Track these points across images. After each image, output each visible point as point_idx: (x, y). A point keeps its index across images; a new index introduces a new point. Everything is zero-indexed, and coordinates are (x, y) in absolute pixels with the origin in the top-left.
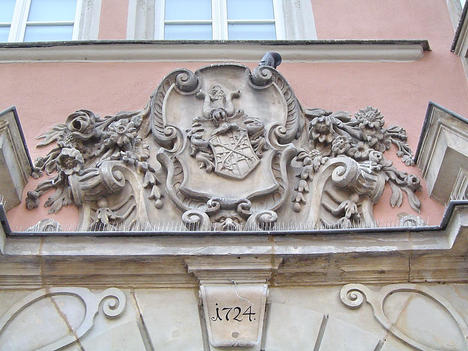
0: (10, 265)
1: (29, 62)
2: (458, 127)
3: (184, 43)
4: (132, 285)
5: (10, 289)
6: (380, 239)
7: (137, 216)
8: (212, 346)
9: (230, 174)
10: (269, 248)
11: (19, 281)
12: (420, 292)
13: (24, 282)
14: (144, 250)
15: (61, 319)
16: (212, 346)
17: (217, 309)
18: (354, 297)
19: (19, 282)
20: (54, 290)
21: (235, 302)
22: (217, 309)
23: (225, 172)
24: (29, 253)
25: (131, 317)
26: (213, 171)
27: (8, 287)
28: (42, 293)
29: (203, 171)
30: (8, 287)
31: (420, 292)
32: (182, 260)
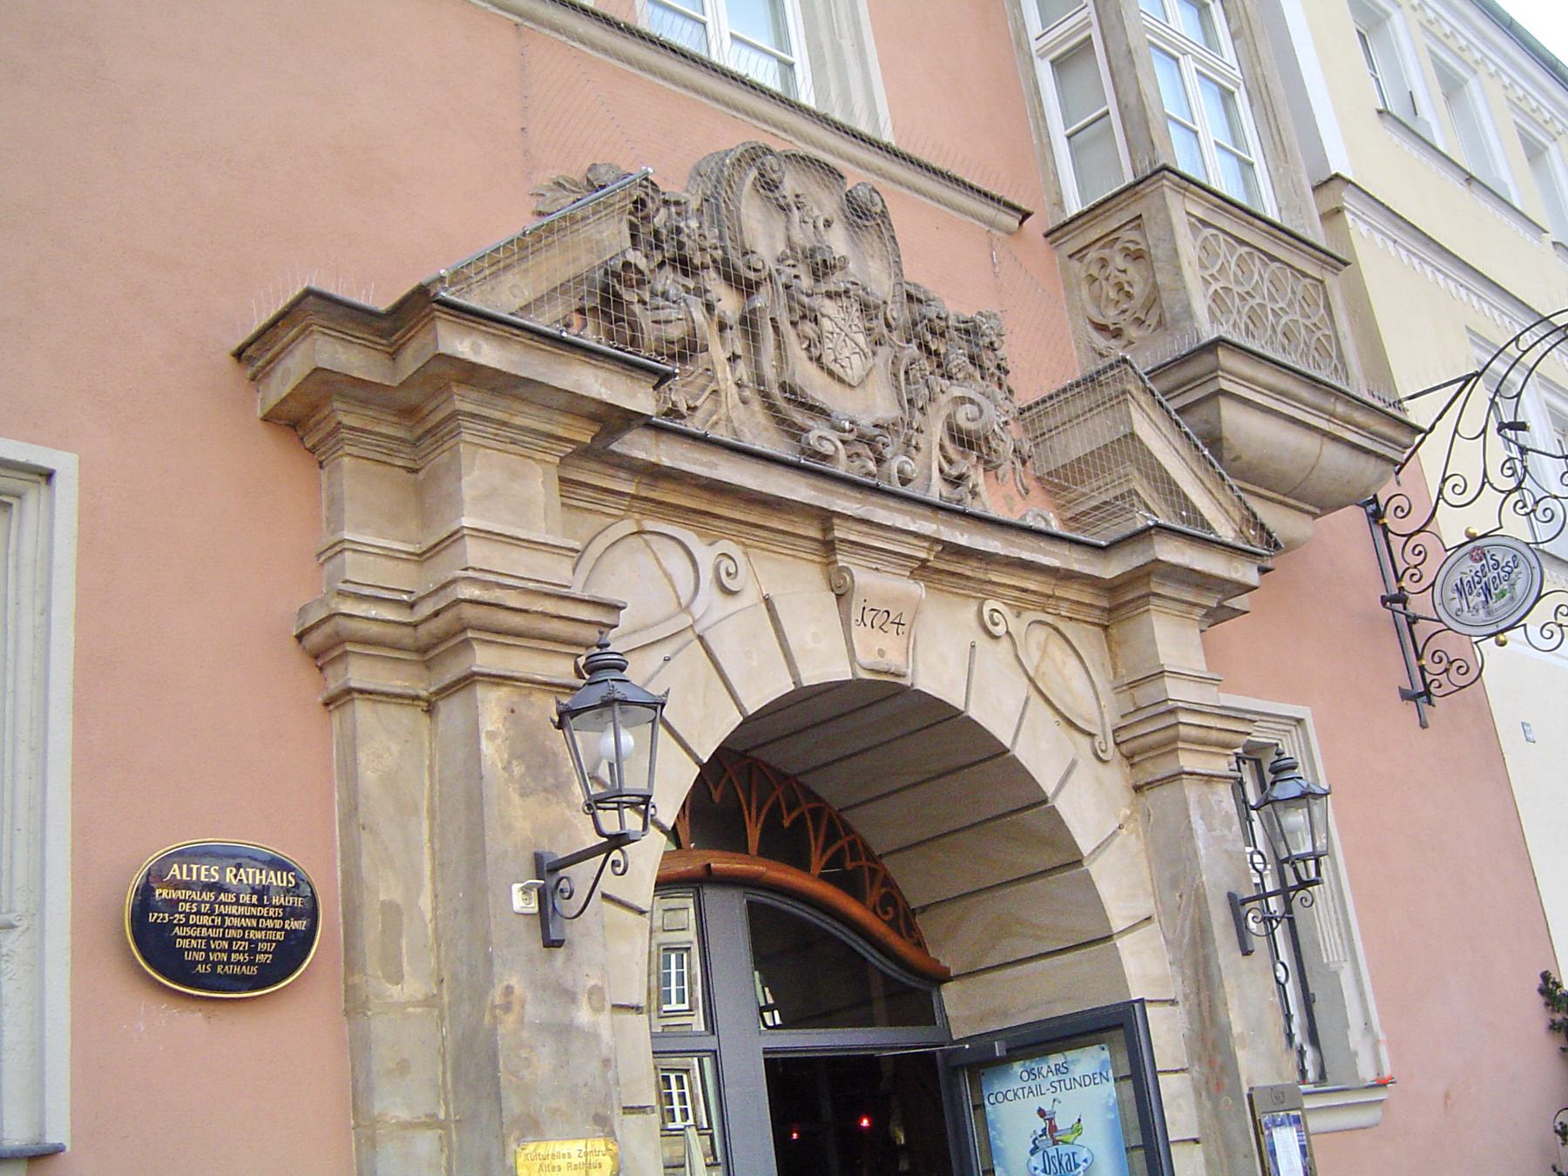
0: (594, 466)
1: (486, 8)
2: (1148, 405)
3: (664, 46)
4: (744, 540)
5: (578, 507)
6: (1042, 544)
7: (723, 410)
8: (860, 665)
9: (840, 372)
10: (934, 526)
11: (595, 495)
12: (1056, 629)
13: (603, 500)
14: (792, 490)
15: (666, 581)
16: (860, 665)
17: (864, 609)
18: (997, 621)
19: (595, 498)
20: (649, 525)
21: (886, 602)
22: (864, 609)
23: (836, 368)
24: (641, 455)
25: (750, 597)
26: (819, 359)
27: (575, 503)
28: (628, 526)
29: (804, 355)
30: (575, 503)
31: (1056, 629)
32: (825, 517)
